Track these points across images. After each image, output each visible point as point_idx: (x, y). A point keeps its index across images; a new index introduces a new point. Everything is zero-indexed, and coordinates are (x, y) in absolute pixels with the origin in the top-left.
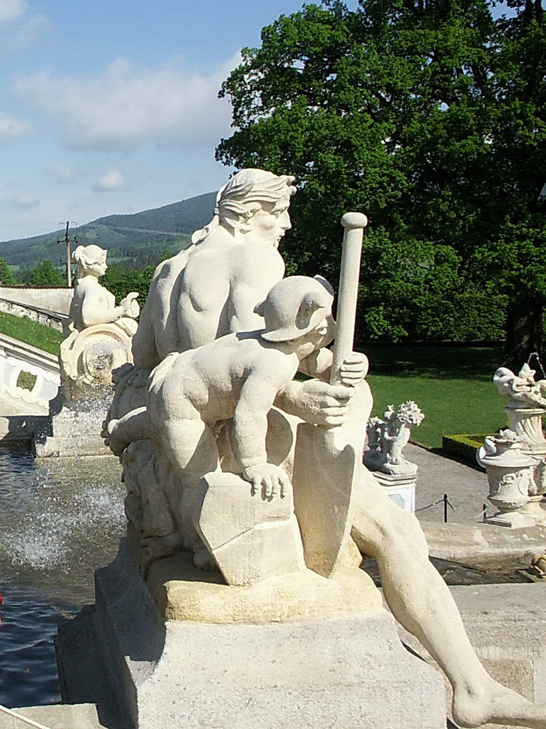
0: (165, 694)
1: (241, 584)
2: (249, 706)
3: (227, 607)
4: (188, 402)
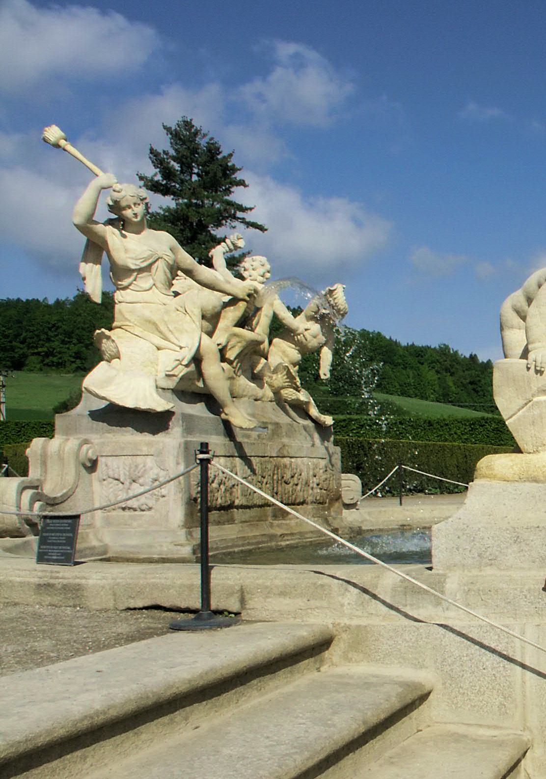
0: (452, 530)
1: (532, 451)
2: (517, 542)
3: (514, 467)
4: (515, 315)
